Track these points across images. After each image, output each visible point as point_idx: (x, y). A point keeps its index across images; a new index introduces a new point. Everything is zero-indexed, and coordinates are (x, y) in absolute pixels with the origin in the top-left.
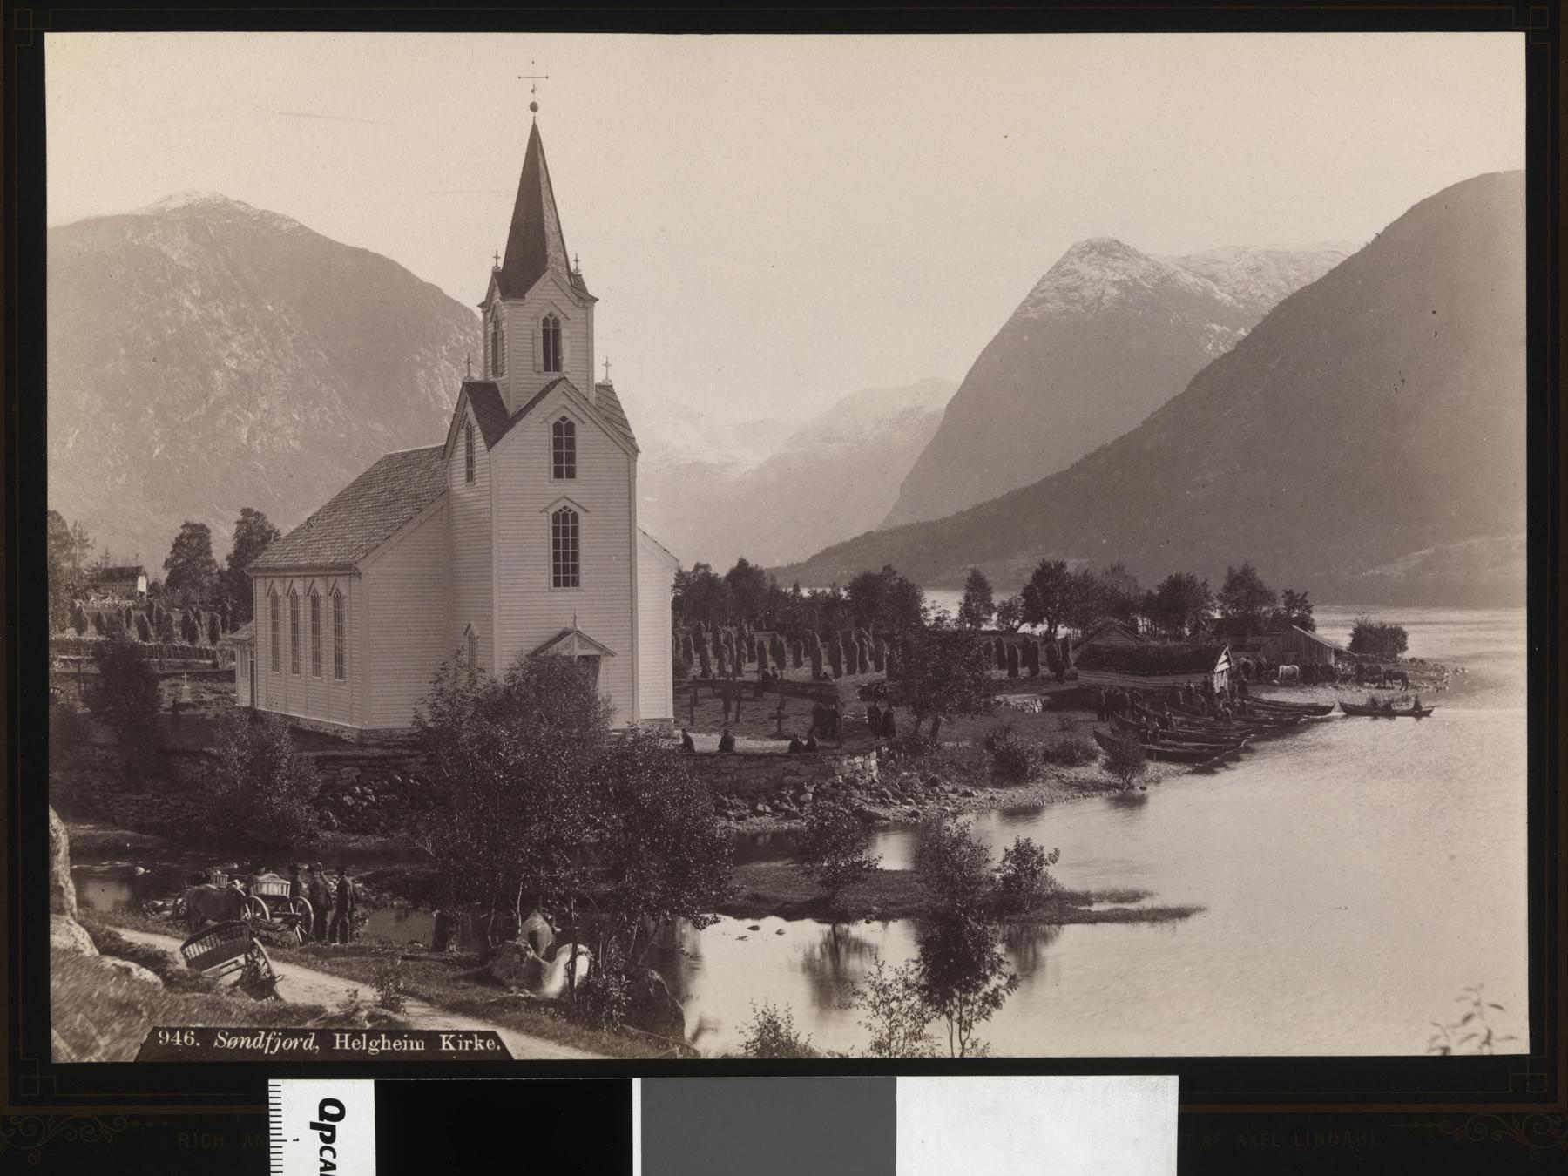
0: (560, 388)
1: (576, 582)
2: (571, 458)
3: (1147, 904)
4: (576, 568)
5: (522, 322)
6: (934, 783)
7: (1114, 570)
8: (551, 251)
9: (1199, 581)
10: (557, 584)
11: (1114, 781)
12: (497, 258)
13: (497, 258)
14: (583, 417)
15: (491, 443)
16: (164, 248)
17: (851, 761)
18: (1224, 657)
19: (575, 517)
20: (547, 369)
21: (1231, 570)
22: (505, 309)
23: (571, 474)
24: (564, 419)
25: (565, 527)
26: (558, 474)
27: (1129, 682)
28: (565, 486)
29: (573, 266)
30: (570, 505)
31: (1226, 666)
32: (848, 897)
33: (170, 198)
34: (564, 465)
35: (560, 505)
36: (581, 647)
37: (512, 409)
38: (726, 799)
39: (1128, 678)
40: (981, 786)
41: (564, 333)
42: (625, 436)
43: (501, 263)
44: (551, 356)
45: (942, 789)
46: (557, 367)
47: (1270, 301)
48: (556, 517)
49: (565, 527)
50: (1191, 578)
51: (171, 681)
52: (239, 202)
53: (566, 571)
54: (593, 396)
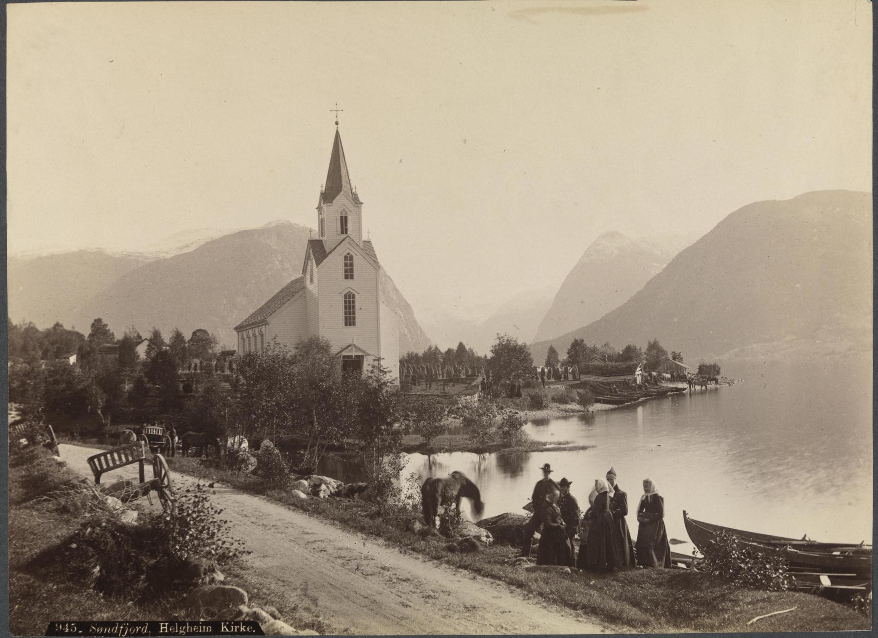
0: (347, 240)
1: (354, 324)
2: (352, 270)
3: (570, 445)
4: (354, 318)
5: (333, 211)
6: (502, 408)
7: (605, 345)
8: (344, 183)
9: (638, 348)
10: (346, 324)
11: (581, 409)
12: (322, 187)
13: (322, 187)
14: (356, 253)
15: (317, 266)
16: (269, 242)
17: (465, 398)
18: (639, 369)
19: (354, 296)
20: (342, 233)
21: (649, 343)
22: (324, 207)
23: (352, 277)
24: (349, 254)
25: (349, 301)
26: (346, 277)
27: (601, 379)
28: (349, 282)
29: (354, 190)
30: (351, 291)
31: (640, 372)
32: (434, 442)
33: (270, 223)
34: (349, 274)
35: (347, 291)
36: (356, 352)
37: (328, 251)
38: (409, 413)
39: (600, 377)
40: (522, 410)
41: (350, 218)
42: (375, 262)
43: (324, 189)
44: (344, 229)
45: (505, 411)
46: (346, 233)
47: (674, 253)
48: (345, 295)
49: (349, 301)
50: (635, 348)
51: (475, 542)
52: (295, 224)
53: (350, 319)
54: (361, 245)
